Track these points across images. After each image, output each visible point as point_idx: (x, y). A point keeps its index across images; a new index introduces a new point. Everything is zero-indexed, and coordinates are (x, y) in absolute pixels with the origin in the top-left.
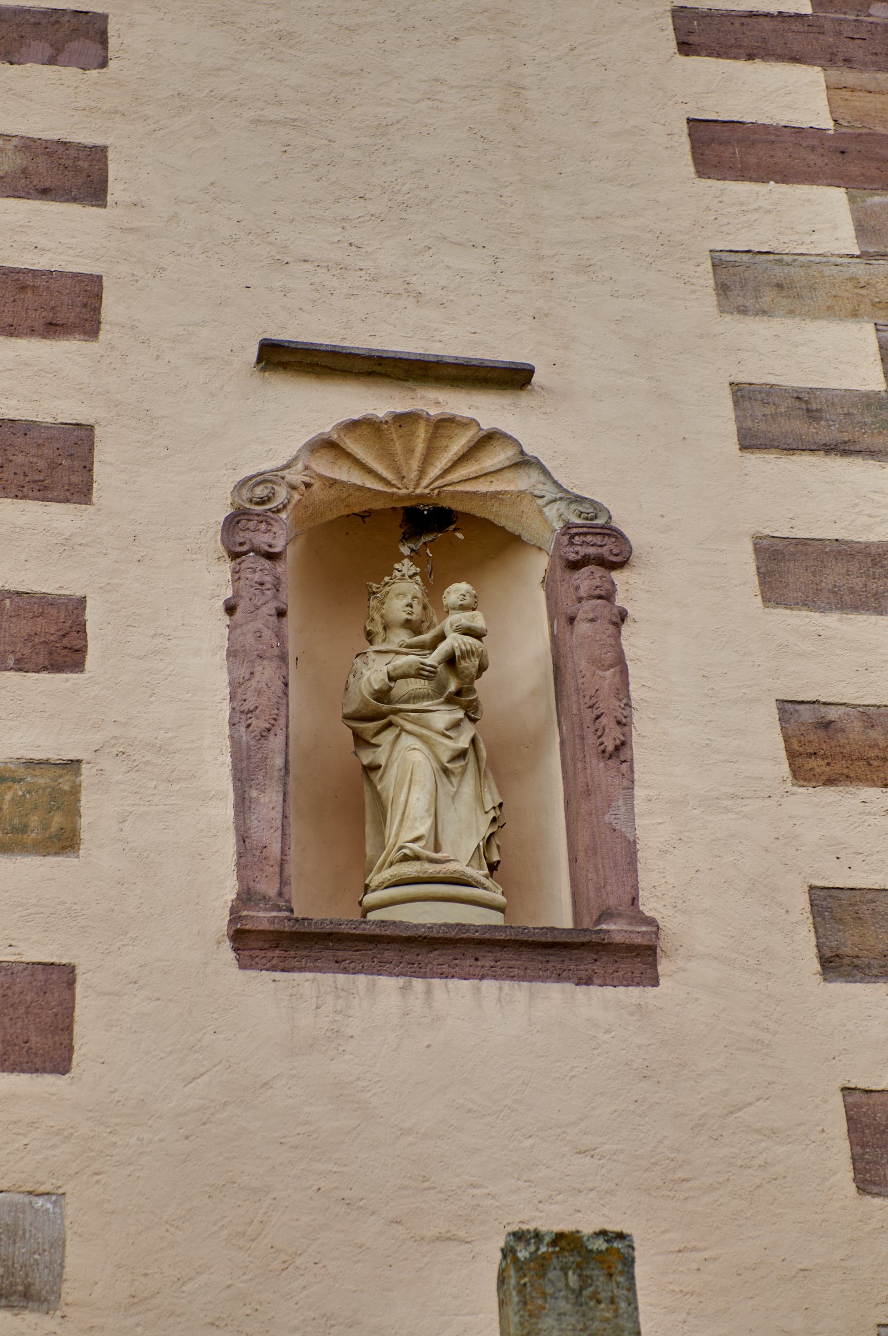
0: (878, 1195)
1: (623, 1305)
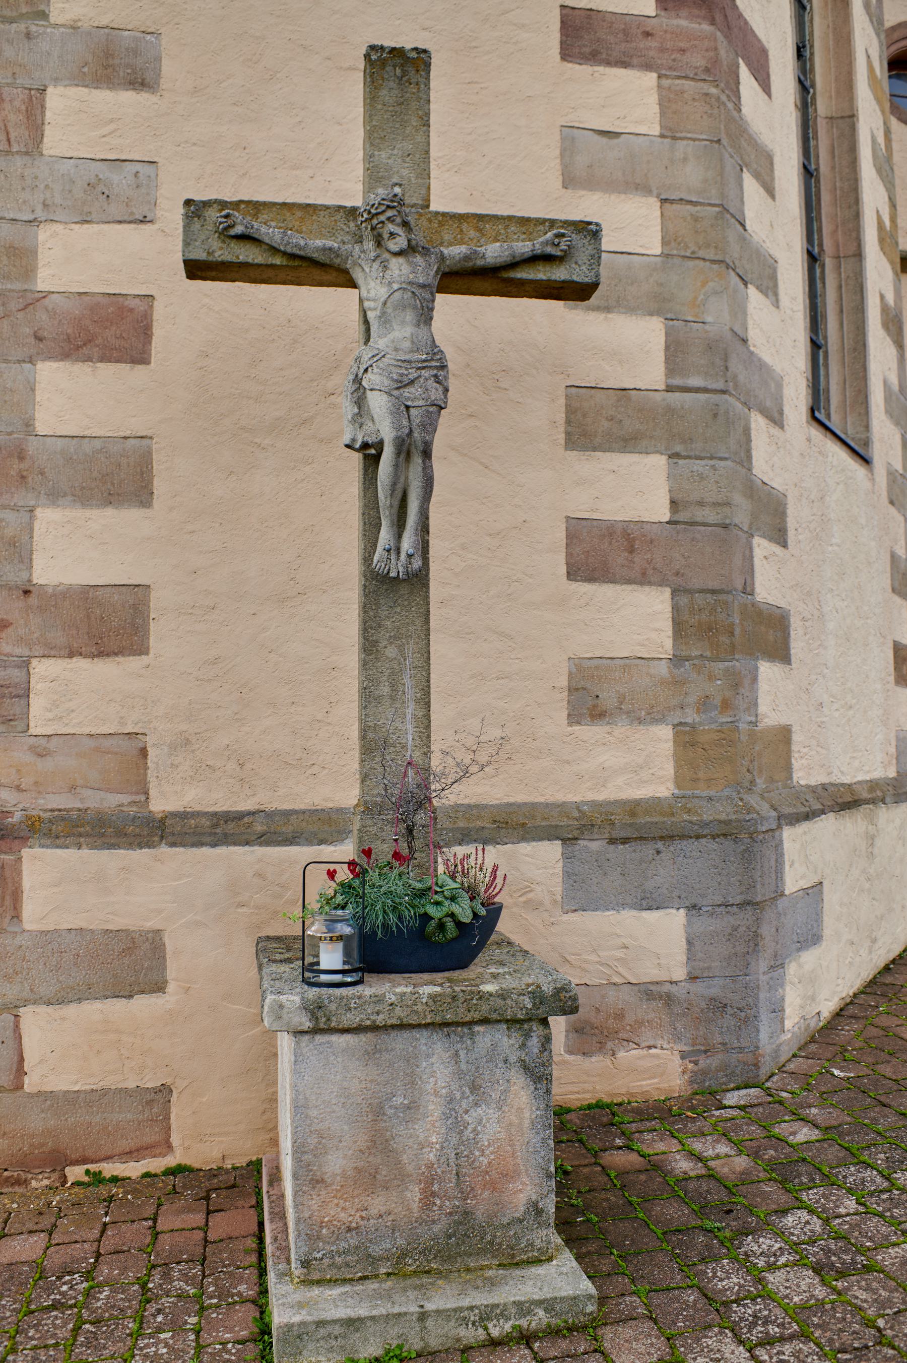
0: (571, 62)
1: (423, 86)
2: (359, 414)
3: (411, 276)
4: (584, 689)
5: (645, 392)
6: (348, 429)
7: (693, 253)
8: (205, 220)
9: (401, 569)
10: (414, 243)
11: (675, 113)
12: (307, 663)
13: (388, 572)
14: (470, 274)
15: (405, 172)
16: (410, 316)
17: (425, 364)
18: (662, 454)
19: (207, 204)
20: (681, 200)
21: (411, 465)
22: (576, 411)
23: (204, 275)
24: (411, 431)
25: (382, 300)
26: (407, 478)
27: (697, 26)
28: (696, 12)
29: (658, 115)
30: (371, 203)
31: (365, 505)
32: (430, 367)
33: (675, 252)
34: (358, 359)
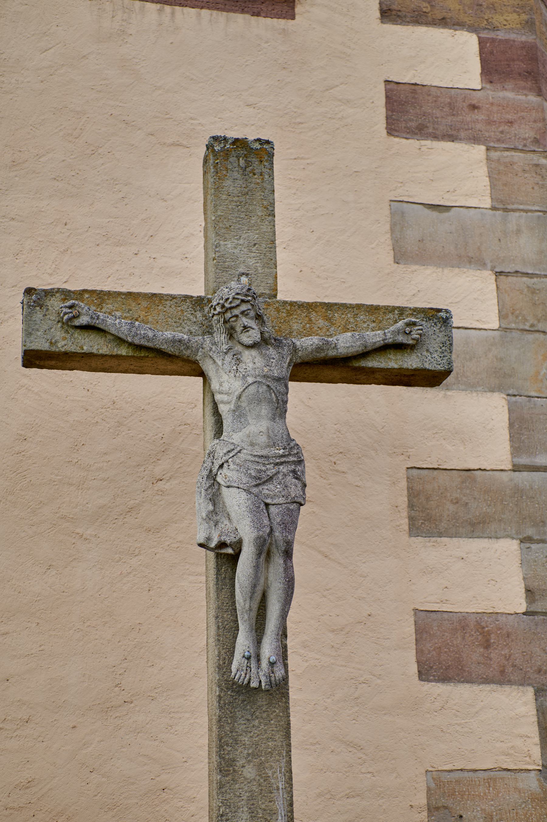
0: (397, 136)
1: (267, 177)
2: (214, 512)
3: (266, 369)
4: (446, 808)
5: (490, 473)
6: (202, 526)
7: (532, 326)
8: (48, 309)
9: (263, 679)
10: (267, 335)
11: (505, 185)
12: (133, 784)
13: (249, 682)
14: (320, 364)
15: (251, 262)
16: (265, 410)
17: (283, 460)
18: (513, 538)
19: (49, 293)
20: (517, 272)
21: (271, 565)
22: (418, 495)
23: (42, 363)
24: (272, 530)
25: (237, 393)
26: (267, 579)
27: (523, 98)
28: (522, 83)
29: (489, 188)
30: (225, 297)
31: (219, 607)
32: (288, 462)
33: (513, 326)
34: (212, 454)
